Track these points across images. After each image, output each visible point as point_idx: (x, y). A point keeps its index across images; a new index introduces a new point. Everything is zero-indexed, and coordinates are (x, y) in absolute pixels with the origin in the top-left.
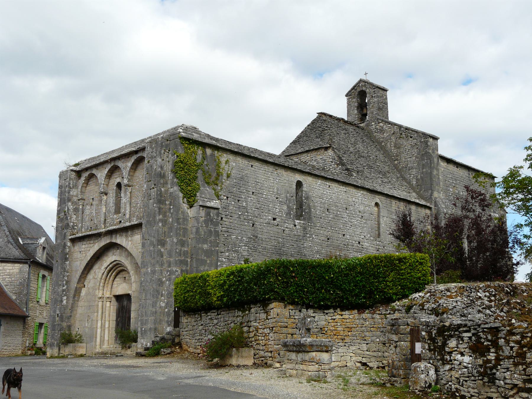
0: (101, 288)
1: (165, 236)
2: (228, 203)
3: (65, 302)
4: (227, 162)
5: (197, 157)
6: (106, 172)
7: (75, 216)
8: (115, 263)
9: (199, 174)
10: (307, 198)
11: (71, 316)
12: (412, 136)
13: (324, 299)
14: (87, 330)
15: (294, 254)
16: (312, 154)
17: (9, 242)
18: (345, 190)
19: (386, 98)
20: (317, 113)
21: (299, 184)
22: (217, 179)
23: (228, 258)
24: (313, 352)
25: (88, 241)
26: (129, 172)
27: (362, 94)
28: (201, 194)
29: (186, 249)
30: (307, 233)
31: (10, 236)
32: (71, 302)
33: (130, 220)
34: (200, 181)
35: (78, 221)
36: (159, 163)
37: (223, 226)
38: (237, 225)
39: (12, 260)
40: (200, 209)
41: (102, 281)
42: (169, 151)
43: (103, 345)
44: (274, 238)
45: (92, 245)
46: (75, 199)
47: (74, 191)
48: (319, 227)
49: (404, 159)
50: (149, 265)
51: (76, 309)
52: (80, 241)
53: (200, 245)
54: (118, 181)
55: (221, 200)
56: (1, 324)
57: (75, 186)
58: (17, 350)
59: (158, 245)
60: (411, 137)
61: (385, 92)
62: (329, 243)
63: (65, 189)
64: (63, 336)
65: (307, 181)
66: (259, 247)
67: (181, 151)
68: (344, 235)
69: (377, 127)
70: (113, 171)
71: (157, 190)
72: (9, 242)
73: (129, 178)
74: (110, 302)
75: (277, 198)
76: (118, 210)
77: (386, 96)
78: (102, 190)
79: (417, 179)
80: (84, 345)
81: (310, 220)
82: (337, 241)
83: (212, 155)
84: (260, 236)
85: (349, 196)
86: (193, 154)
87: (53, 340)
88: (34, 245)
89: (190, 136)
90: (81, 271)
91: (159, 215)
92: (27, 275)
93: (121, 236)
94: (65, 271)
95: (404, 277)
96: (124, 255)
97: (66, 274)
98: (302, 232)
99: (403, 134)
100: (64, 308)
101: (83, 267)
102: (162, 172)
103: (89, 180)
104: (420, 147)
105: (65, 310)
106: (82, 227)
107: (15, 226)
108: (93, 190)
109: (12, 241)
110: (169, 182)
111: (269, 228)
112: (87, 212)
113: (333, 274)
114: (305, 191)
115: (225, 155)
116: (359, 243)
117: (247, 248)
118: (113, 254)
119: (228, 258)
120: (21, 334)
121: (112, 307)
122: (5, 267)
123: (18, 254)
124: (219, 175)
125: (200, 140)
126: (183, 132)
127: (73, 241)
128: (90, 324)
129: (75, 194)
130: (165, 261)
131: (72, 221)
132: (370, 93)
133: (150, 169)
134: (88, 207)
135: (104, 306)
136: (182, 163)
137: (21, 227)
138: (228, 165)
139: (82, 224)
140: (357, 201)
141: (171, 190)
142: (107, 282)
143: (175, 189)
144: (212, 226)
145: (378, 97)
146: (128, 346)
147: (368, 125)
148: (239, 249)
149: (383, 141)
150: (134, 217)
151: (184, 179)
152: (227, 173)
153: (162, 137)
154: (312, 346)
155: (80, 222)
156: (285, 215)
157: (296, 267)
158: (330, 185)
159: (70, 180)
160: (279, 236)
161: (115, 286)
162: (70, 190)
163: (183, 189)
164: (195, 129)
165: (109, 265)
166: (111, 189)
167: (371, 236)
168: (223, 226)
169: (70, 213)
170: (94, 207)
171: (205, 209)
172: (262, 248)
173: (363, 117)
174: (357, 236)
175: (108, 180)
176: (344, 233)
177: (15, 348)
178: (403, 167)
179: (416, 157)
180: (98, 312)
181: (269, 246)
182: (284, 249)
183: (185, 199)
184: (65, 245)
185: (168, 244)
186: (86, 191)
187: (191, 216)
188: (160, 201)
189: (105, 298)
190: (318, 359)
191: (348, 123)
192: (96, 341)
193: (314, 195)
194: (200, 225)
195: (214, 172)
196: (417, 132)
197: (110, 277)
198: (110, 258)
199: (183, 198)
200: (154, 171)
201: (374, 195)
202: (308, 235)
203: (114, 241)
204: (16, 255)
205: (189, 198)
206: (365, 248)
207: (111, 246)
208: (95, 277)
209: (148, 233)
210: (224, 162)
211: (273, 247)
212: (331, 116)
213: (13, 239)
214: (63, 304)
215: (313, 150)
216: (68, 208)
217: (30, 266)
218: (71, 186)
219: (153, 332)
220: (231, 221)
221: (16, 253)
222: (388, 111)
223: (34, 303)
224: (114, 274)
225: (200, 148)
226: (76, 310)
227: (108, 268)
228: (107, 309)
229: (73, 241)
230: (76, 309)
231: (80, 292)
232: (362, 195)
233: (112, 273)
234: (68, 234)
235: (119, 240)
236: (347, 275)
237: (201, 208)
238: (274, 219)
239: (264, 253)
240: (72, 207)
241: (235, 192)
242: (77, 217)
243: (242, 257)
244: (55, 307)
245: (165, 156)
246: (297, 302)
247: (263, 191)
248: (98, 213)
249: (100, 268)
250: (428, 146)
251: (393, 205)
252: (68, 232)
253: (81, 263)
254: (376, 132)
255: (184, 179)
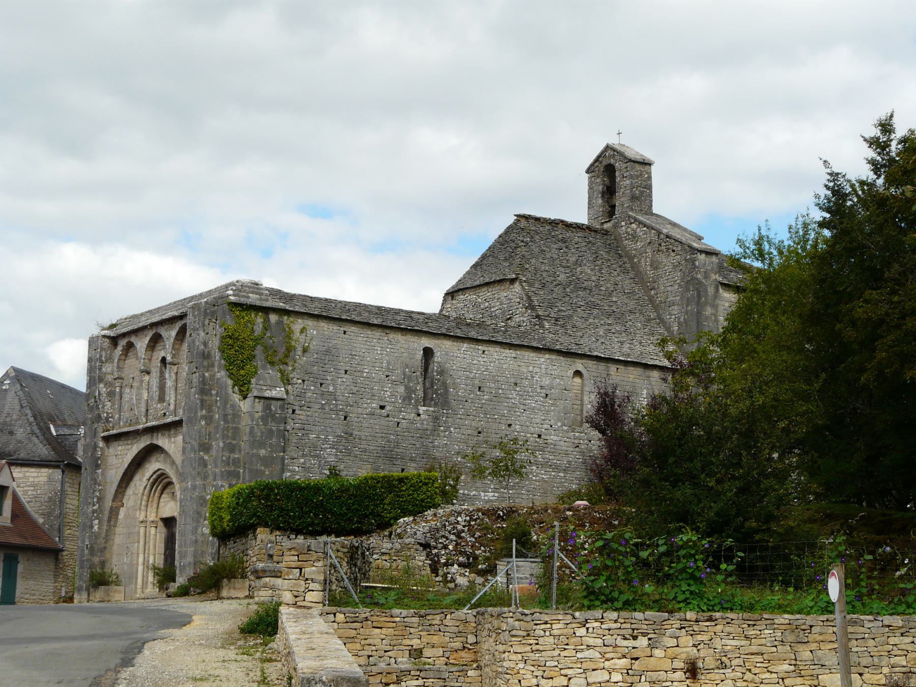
0: (143, 508)
1: (210, 439)
2: (304, 389)
3: (96, 527)
4: (303, 330)
5: (255, 328)
6: (147, 342)
7: (109, 404)
8: (159, 473)
9: (259, 351)
10: (442, 372)
11: (105, 548)
12: (674, 248)
13: (312, 524)
14: (126, 567)
15: (416, 457)
16: (494, 289)
17: (33, 433)
18: (514, 355)
19: (650, 178)
20: (515, 215)
21: (428, 353)
22: (287, 356)
23: (303, 465)
24: (267, 577)
25: (125, 440)
26: (174, 344)
27: (610, 170)
28: (259, 380)
29: (236, 456)
30: (441, 424)
31: (35, 424)
32: (105, 527)
33: (175, 413)
34: (259, 362)
35: (114, 410)
36: (201, 338)
37: (296, 421)
38: (318, 420)
39: (36, 462)
40: (254, 401)
41: (145, 498)
42: (216, 320)
43: (146, 589)
44: (380, 435)
45: (130, 446)
46: (110, 378)
47: (108, 367)
48: (462, 415)
49: (663, 288)
50: (189, 477)
51: (112, 538)
52: (116, 441)
53: (255, 451)
54: (163, 355)
55: (294, 385)
56: (19, 560)
57: (110, 359)
58: (46, 602)
59: (200, 451)
60: (674, 251)
61: (648, 167)
62: (480, 438)
63: (96, 363)
64: (92, 576)
65: (442, 348)
66: (354, 449)
67: (230, 323)
68: (510, 425)
69: (629, 230)
70: (157, 340)
71: (199, 375)
72: (33, 433)
73: (173, 352)
74: (156, 527)
75: (387, 376)
76: (162, 399)
77: (650, 174)
78: (142, 368)
79: (679, 323)
80: (122, 588)
81: (445, 406)
82: (495, 435)
83: (279, 323)
84: (357, 433)
85: (522, 364)
86: (249, 324)
87: (81, 583)
88: (74, 436)
89: (243, 300)
90: (117, 484)
91: (202, 410)
92: (60, 486)
93: (163, 435)
94: (95, 484)
95: (404, 499)
96: (168, 462)
97: (97, 487)
98: (432, 424)
99: (663, 244)
100: (95, 536)
101: (119, 478)
102: (206, 351)
103: (128, 349)
104: (684, 270)
105: (96, 539)
106: (120, 419)
107: (44, 405)
108: (133, 366)
109: (37, 431)
110: (216, 364)
111: (371, 421)
112: (126, 397)
113: (323, 497)
114: (438, 363)
115: (299, 321)
116: (540, 436)
117: (334, 450)
118: (157, 460)
119: (303, 465)
120: (52, 577)
121: (158, 534)
122: (27, 474)
123: (47, 453)
124: (290, 350)
125: (258, 303)
126: (234, 295)
127: (107, 439)
128: (129, 559)
129: (109, 370)
130: (210, 472)
131: (106, 411)
132: (620, 170)
133: (192, 346)
134: (127, 390)
135: (147, 533)
136: (231, 338)
137: (56, 405)
138: (304, 334)
139: (120, 415)
140: (538, 370)
141: (218, 375)
142: (150, 500)
143: (222, 374)
144: (273, 424)
145: (631, 177)
146: (165, 587)
147: (616, 226)
148: (322, 452)
149: (635, 256)
150: (180, 408)
151: (234, 361)
152: (303, 347)
153: (206, 303)
154: (264, 571)
155: (117, 411)
156: (400, 401)
157: (282, 489)
158: (486, 349)
159: (101, 351)
160: (390, 432)
161: (161, 504)
162: (101, 365)
163: (232, 374)
164: (255, 287)
165: (152, 476)
166: (154, 365)
167: (563, 425)
168: (296, 421)
169: (102, 399)
170: (134, 391)
171: (262, 401)
172: (360, 450)
173: (611, 212)
174: (535, 425)
175: (150, 352)
176: (509, 422)
177: (42, 598)
178: (661, 302)
179: (680, 286)
180: (138, 542)
181: (372, 448)
182: (398, 450)
183: (236, 387)
184: (95, 446)
185: (214, 449)
186: (125, 366)
187: (244, 410)
188: (204, 390)
189: (148, 523)
190: (272, 584)
191: (573, 228)
192: (136, 584)
193: (454, 368)
194: (254, 423)
195: (282, 347)
196: (681, 242)
197: (155, 491)
198: (153, 466)
199: (234, 387)
200: (196, 348)
201: (572, 359)
202: (442, 428)
203: (155, 442)
204: (43, 454)
205: (241, 386)
206: (552, 444)
207: (151, 451)
208: (136, 492)
209: (189, 434)
210: (299, 330)
211: (379, 448)
212: (537, 219)
213: (40, 428)
214: (93, 531)
215: (495, 282)
216: (99, 392)
217: (63, 472)
218: (103, 359)
219: (192, 567)
220: (309, 413)
221: (43, 451)
222: (652, 201)
223: (74, 529)
224: (159, 488)
225: (260, 314)
226: (113, 540)
227: (151, 480)
228: (152, 537)
229: (107, 439)
230: (112, 538)
231: (118, 514)
232: (548, 361)
233: (157, 487)
234: (100, 429)
235: (162, 441)
236: (338, 498)
237: (257, 400)
238: (382, 407)
239: (363, 457)
240: (105, 389)
241: (315, 372)
242: (113, 404)
243: (326, 464)
244: (84, 536)
245: (211, 328)
246: (284, 527)
247: (363, 367)
248: (139, 400)
249: (141, 480)
250: (695, 267)
251: (613, 373)
252: (100, 427)
253: (116, 472)
254: (626, 240)
255: (234, 361)
